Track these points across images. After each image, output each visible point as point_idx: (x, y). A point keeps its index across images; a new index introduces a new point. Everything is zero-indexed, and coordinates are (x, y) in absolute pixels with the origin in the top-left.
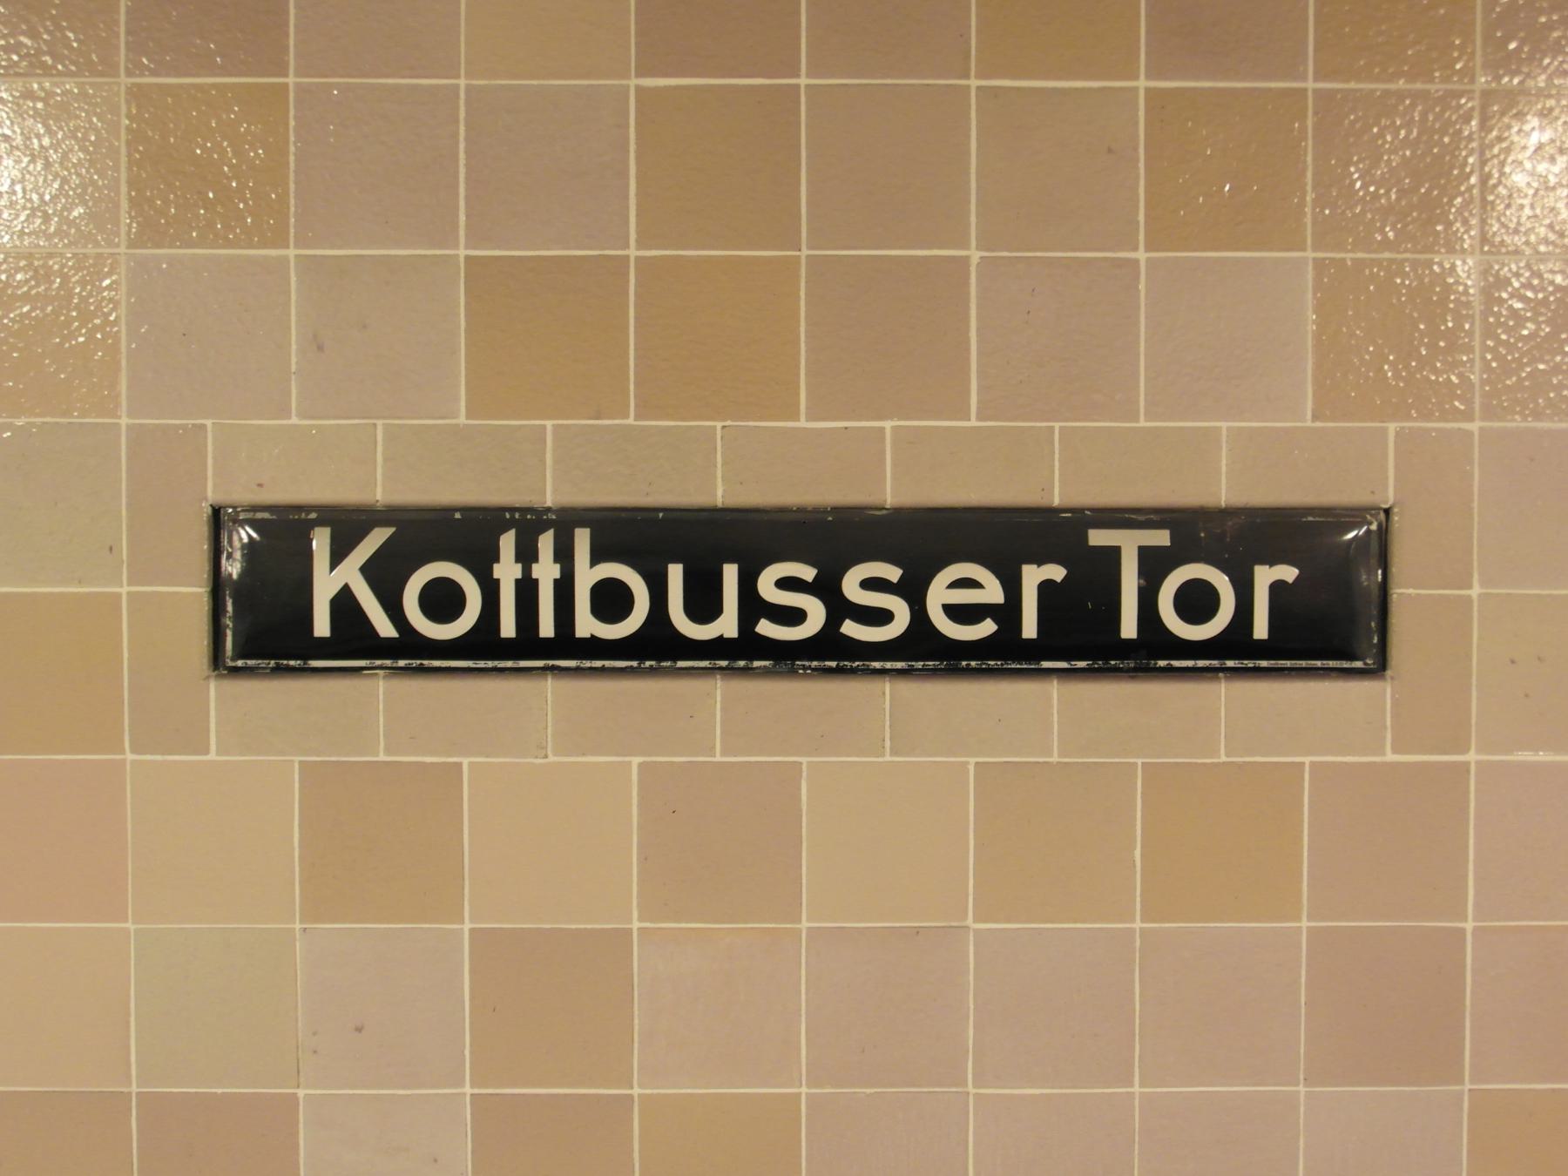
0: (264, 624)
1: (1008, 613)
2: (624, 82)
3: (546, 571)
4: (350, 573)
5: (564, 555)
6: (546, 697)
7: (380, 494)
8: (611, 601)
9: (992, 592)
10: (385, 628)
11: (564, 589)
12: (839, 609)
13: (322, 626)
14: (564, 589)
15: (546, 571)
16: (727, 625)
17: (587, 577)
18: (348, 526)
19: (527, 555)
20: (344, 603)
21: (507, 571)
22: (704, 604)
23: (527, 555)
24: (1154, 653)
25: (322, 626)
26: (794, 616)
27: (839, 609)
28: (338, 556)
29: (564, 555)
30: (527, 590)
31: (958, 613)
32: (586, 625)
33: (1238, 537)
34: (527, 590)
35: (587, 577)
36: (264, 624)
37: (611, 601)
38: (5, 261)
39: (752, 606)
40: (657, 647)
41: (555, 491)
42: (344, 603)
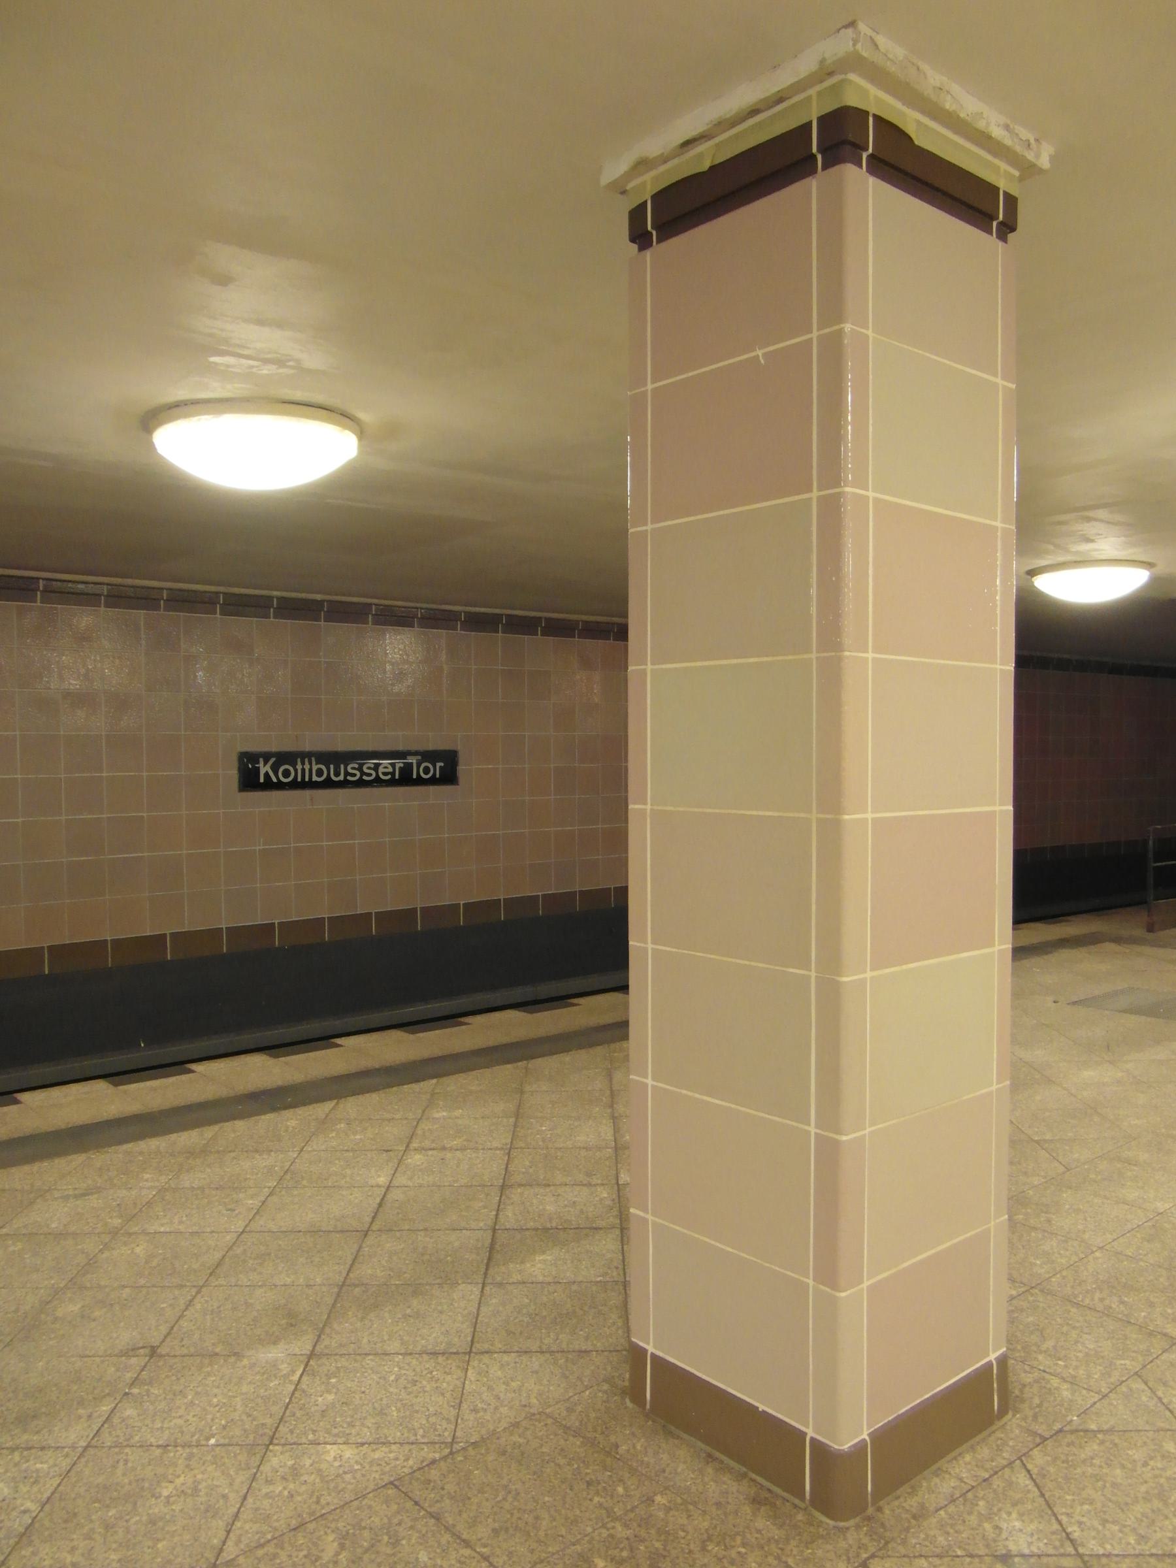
0: (250, 781)
1: (393, 774)
2: (862, 976)
3: (307, 767)
4: (268, 768)
5: (310, 764)
6: (307, 793)
7: (274, 750)
8: (320, 773)
9: (390, 770)
10: (275, 780)
11: (310, 770)
12: (362, 773)
13: (262, 780)
14: (310, 770)
15: (307, 767)
16: (341, 778)
17: (315, 767)
18: (267, 757)
19: (303, 764)
20: (267, 774)
21: (299, 767)
22: (337, 774)
23: (303, 764)
24: (420, 782)
25: (262, 780)
26: (354, 775)
27: (362, 773)
28: (265, 764)
29: (310, 764)
30: (303, 770)
31: (385, 774)
32: (315, 778)
33: (429, 756)
34: (303, 770)
35: (315, 767)
36: (250, 781)
37: (320, 773)
38: (6, 1471)
39: (347, 774)
40: (328, 784)
41: (635, 1215)
42: (267, 774)
